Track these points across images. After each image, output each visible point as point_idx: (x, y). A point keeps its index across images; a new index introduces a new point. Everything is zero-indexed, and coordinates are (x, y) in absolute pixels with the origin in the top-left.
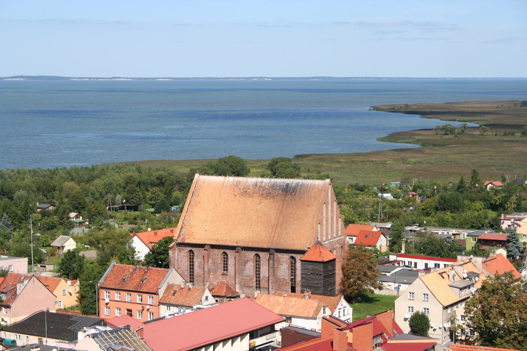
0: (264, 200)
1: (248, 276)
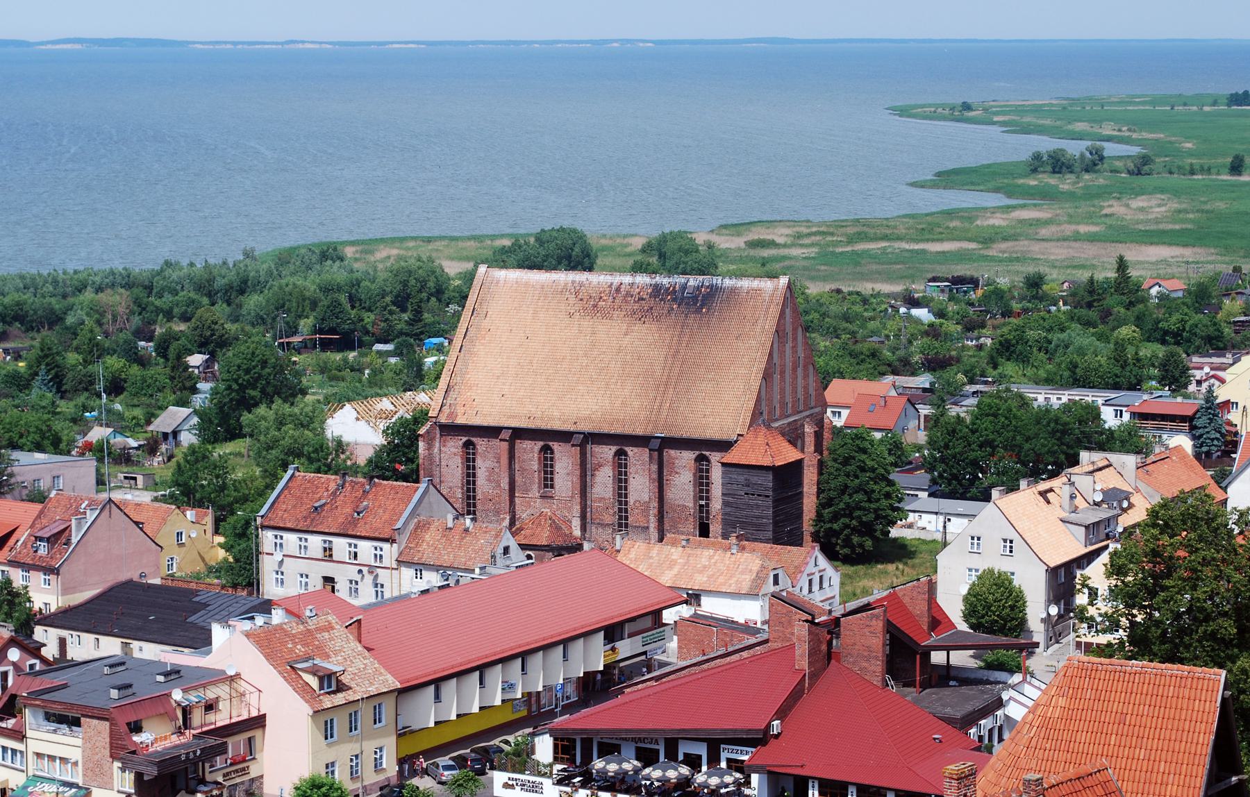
0: (638, 327)
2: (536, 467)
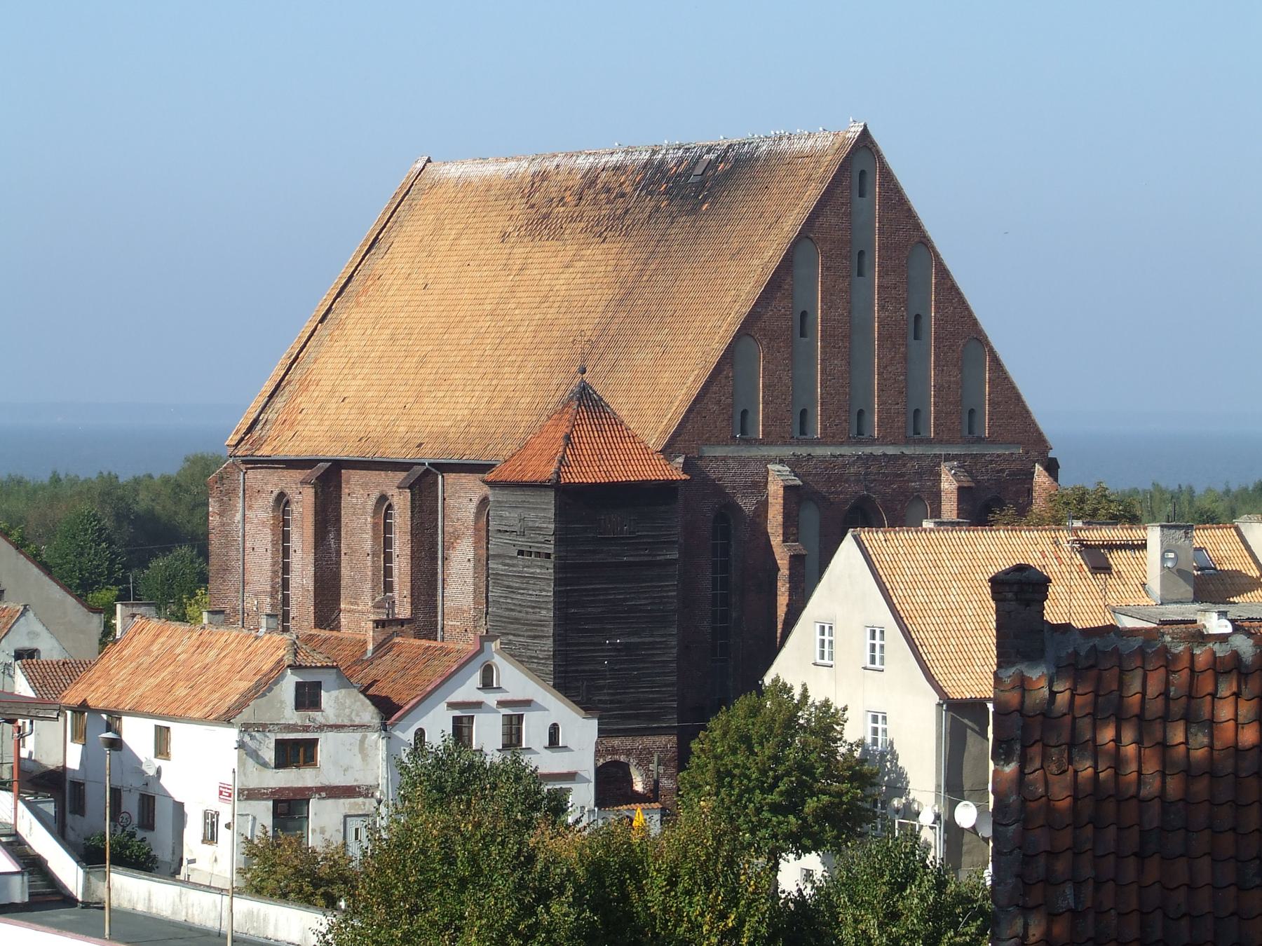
1: (460, 611)
2: (368, 546)
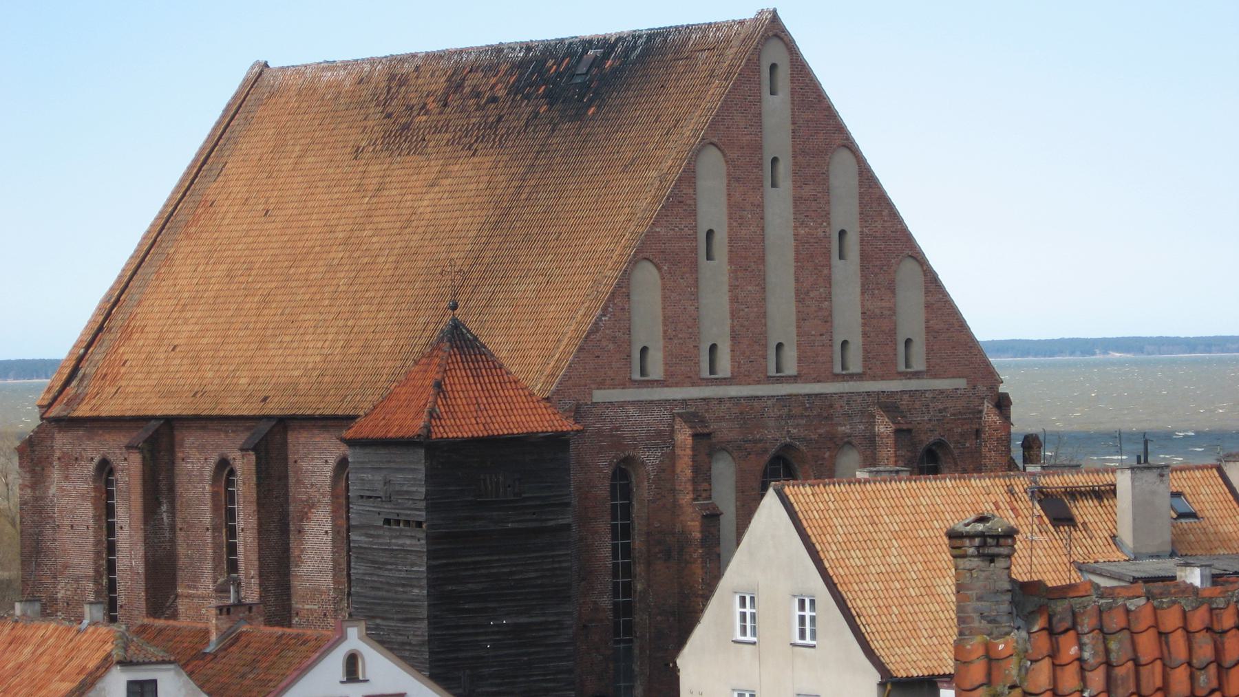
1: (317, 591)
2: (207, 519)
